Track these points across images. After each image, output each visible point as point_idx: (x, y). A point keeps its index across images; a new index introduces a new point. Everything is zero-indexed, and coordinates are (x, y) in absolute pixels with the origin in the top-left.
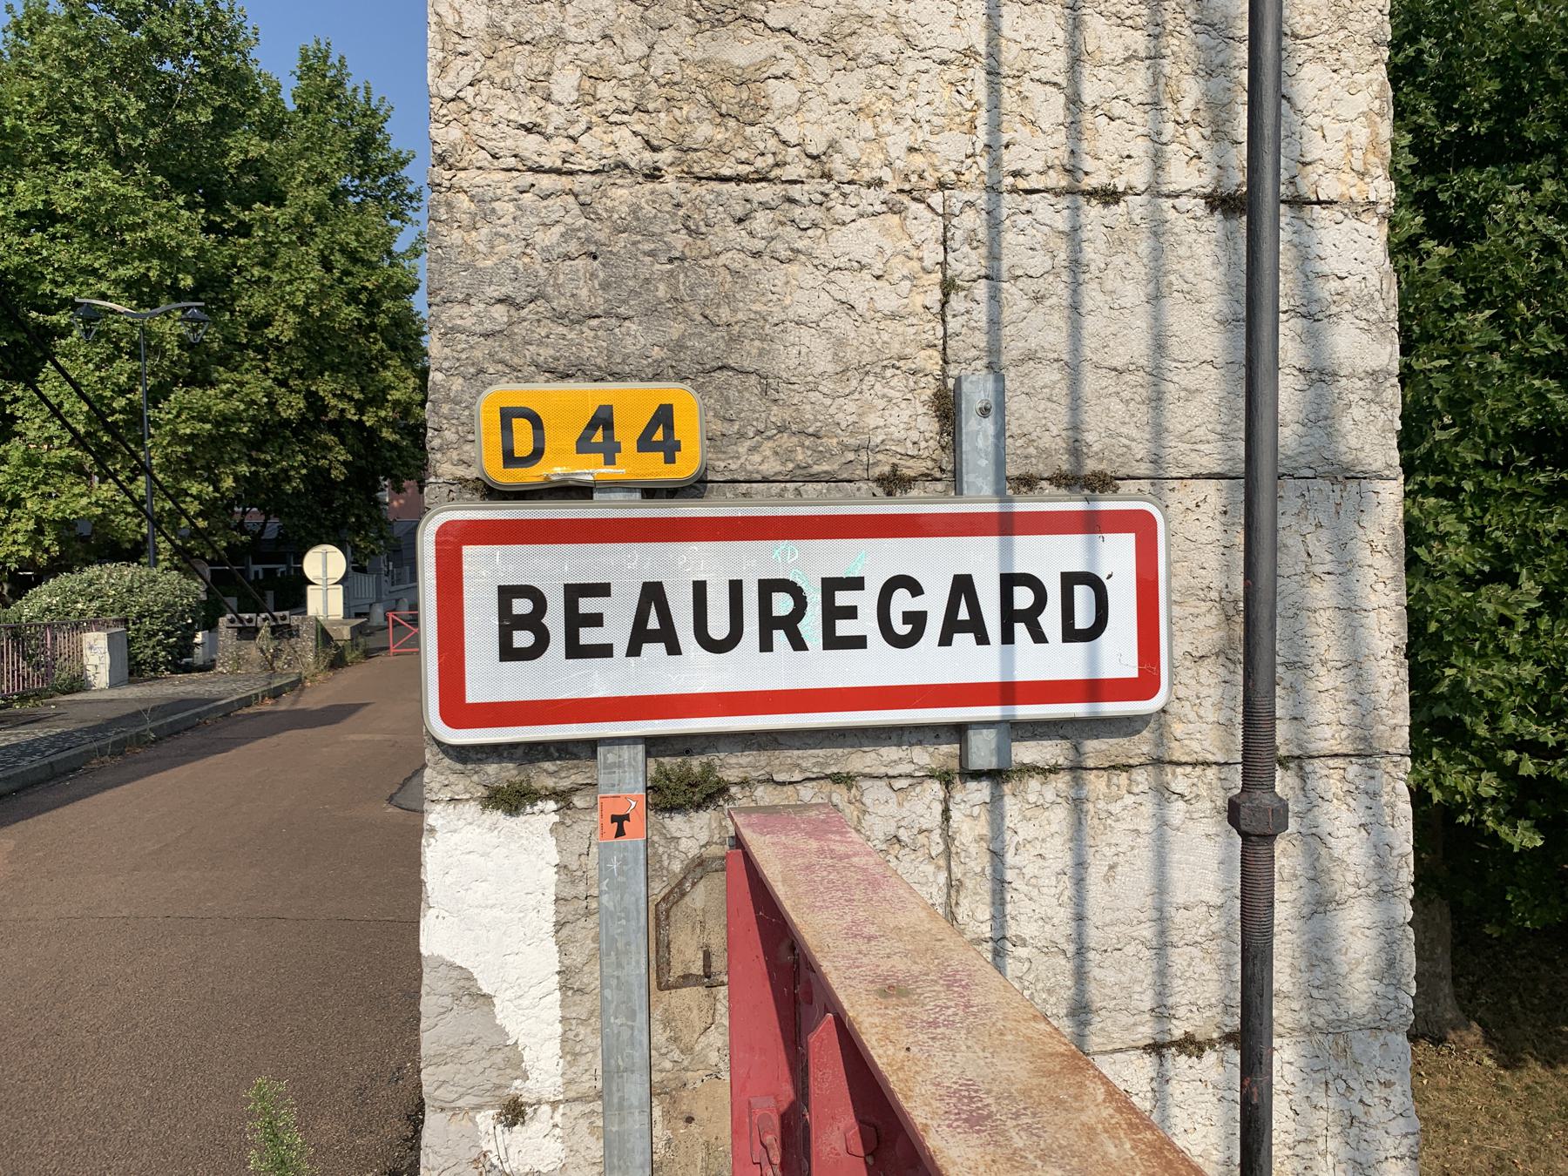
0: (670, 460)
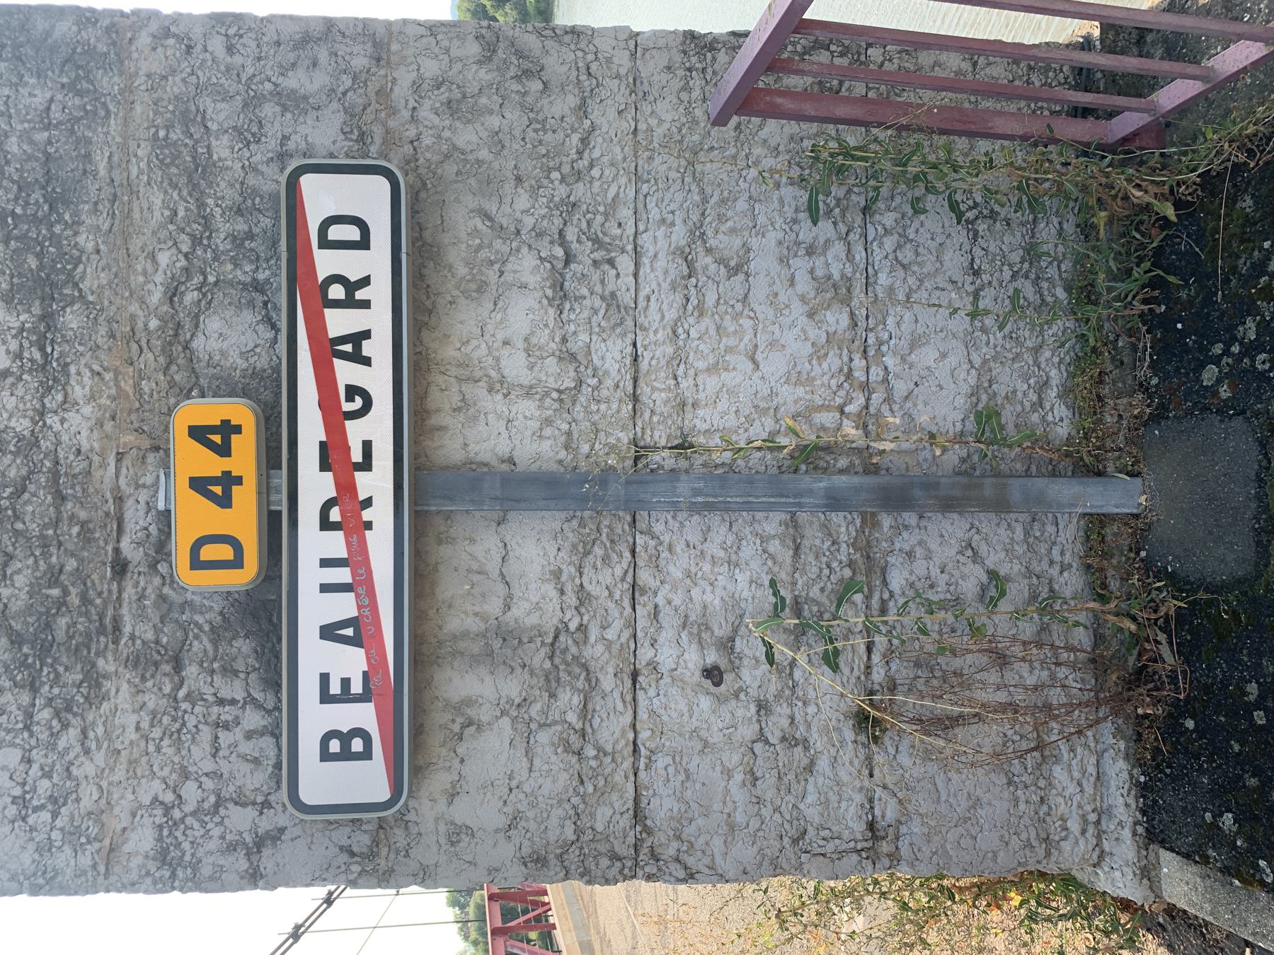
0: (238, 429)
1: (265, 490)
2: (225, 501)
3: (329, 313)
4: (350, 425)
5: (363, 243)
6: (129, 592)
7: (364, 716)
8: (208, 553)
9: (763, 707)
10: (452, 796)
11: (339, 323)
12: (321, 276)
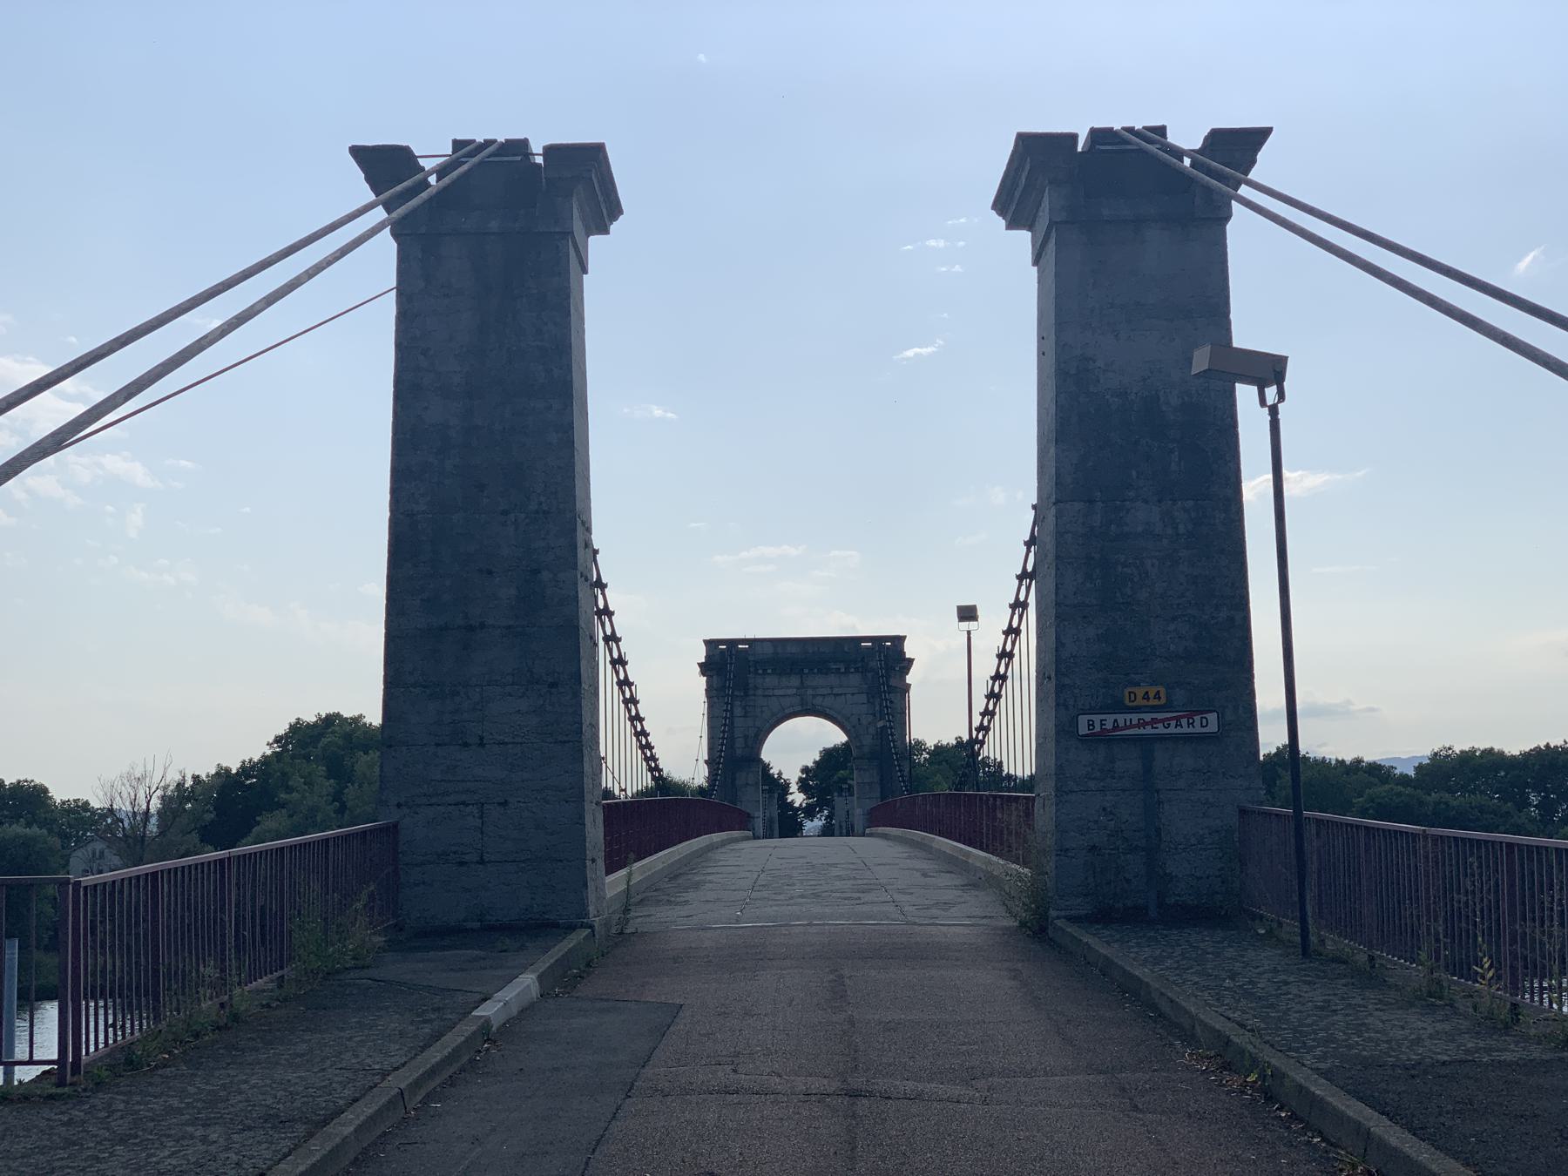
1: (1146, 706)
2: (1144, 698)
3: (1186, 719)
4: (1162, 725)
5: (1202, 726)
6: (1122, 676)
7: (1098, 728)
8: (1132, 695)
9: (1096, 822)
10: (1076, 748)
11: (1184, 722)
12: (1195, 718)
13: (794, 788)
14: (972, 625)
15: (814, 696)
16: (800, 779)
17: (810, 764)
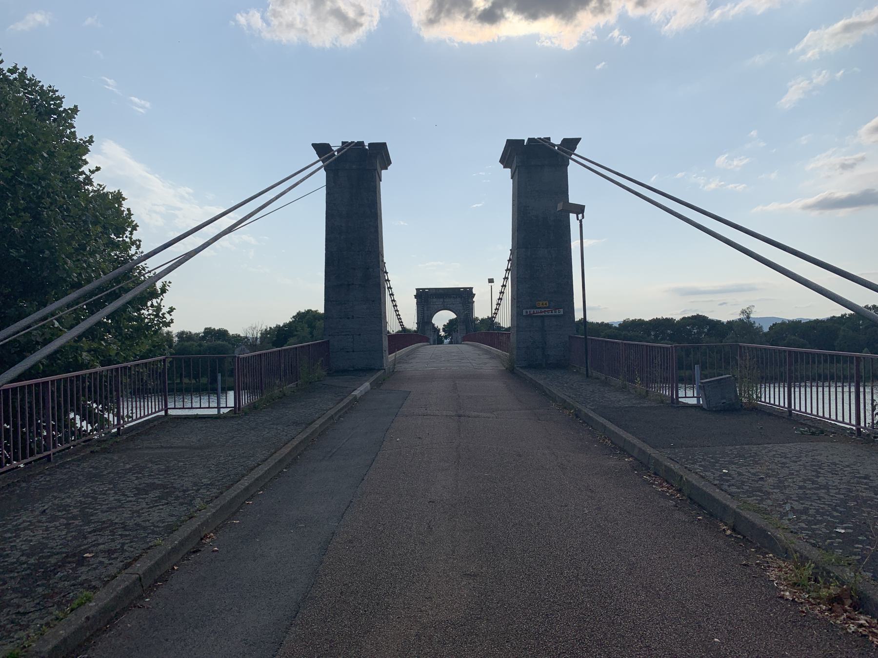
11: (553, 311)
13: (441, 330)
14: (492, 284)
15: (447, 304)
16: (443, 328)
17: (446, 324)
